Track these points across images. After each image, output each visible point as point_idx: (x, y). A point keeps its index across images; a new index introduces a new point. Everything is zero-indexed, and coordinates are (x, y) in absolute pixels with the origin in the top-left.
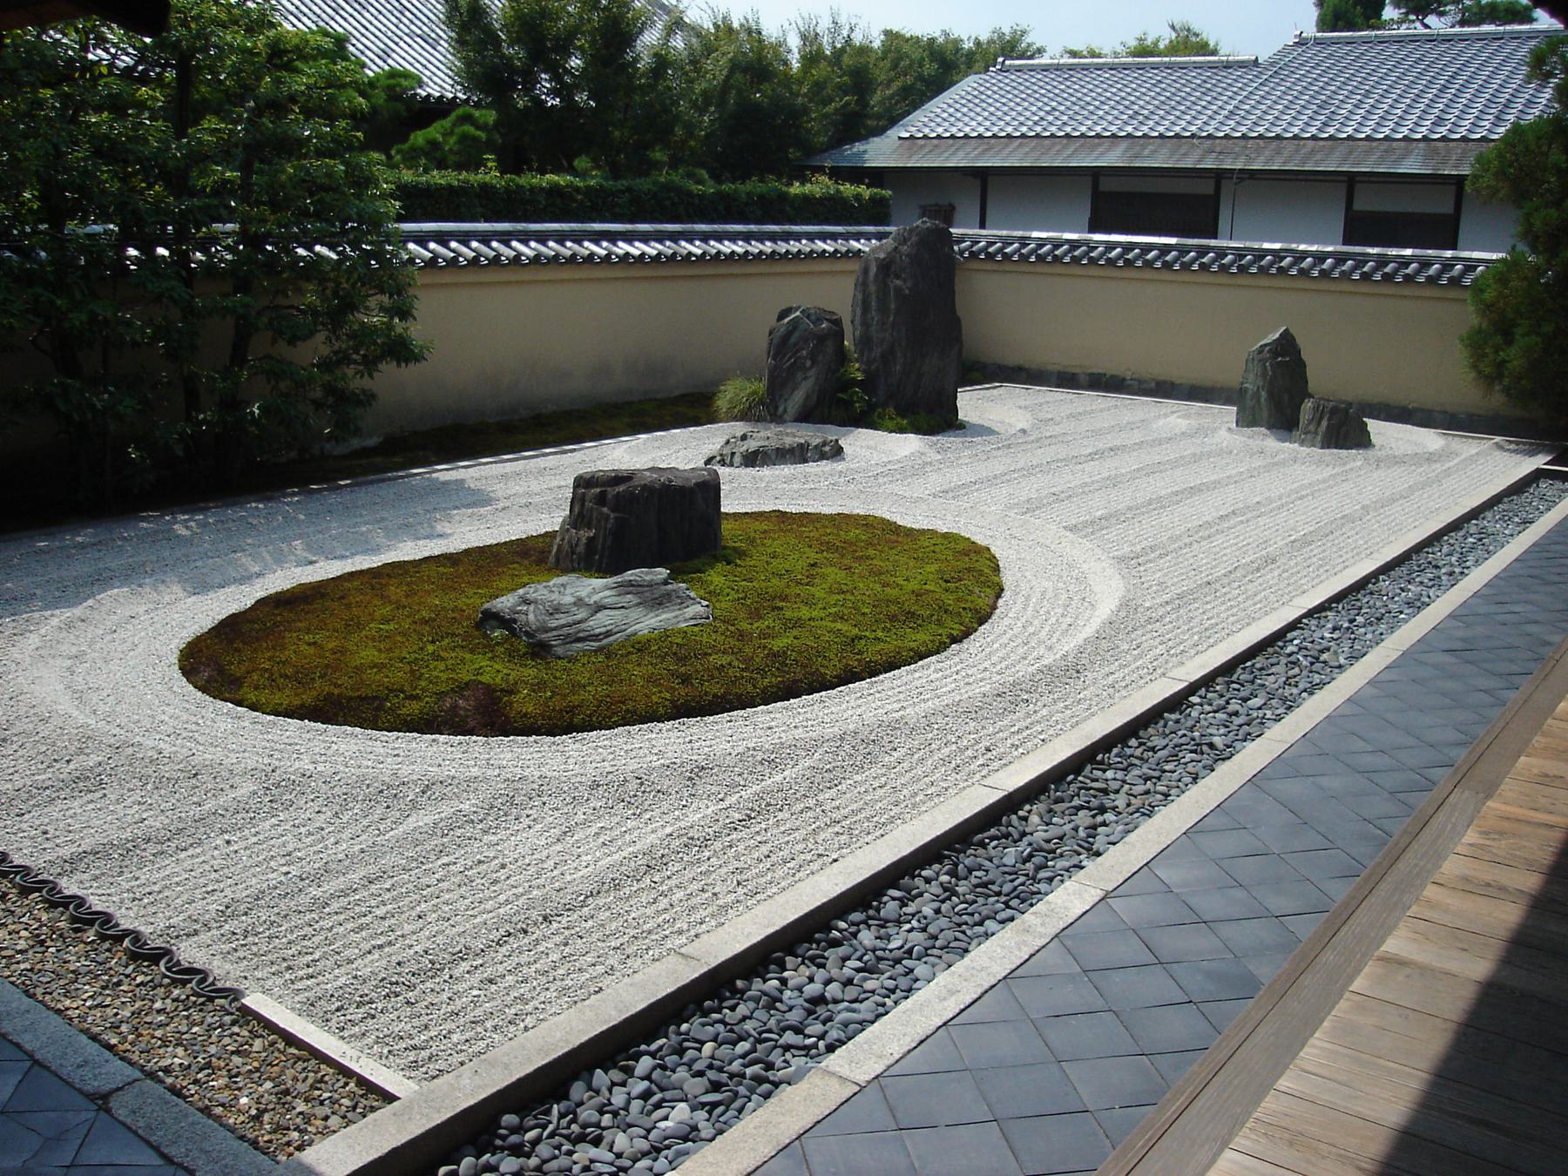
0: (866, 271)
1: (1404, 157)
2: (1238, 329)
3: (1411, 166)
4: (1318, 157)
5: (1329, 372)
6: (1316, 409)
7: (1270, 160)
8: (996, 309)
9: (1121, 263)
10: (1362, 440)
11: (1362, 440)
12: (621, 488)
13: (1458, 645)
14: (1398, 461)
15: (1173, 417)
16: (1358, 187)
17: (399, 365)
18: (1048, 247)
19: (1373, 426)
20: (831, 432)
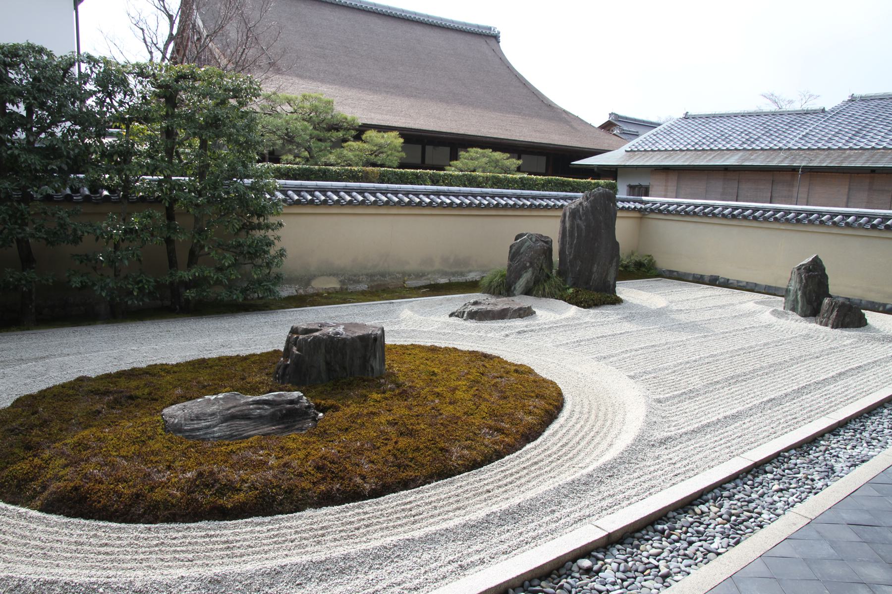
0: (565, 215)
2: (782, 255)
4: (852, 159)
5: (841, 285)
6: (830, 304)
10: (860, 323)
11: (860, 323)
13: (864, 518)
15: (748, 302)
16: (429, 149)
19: (869, 316)
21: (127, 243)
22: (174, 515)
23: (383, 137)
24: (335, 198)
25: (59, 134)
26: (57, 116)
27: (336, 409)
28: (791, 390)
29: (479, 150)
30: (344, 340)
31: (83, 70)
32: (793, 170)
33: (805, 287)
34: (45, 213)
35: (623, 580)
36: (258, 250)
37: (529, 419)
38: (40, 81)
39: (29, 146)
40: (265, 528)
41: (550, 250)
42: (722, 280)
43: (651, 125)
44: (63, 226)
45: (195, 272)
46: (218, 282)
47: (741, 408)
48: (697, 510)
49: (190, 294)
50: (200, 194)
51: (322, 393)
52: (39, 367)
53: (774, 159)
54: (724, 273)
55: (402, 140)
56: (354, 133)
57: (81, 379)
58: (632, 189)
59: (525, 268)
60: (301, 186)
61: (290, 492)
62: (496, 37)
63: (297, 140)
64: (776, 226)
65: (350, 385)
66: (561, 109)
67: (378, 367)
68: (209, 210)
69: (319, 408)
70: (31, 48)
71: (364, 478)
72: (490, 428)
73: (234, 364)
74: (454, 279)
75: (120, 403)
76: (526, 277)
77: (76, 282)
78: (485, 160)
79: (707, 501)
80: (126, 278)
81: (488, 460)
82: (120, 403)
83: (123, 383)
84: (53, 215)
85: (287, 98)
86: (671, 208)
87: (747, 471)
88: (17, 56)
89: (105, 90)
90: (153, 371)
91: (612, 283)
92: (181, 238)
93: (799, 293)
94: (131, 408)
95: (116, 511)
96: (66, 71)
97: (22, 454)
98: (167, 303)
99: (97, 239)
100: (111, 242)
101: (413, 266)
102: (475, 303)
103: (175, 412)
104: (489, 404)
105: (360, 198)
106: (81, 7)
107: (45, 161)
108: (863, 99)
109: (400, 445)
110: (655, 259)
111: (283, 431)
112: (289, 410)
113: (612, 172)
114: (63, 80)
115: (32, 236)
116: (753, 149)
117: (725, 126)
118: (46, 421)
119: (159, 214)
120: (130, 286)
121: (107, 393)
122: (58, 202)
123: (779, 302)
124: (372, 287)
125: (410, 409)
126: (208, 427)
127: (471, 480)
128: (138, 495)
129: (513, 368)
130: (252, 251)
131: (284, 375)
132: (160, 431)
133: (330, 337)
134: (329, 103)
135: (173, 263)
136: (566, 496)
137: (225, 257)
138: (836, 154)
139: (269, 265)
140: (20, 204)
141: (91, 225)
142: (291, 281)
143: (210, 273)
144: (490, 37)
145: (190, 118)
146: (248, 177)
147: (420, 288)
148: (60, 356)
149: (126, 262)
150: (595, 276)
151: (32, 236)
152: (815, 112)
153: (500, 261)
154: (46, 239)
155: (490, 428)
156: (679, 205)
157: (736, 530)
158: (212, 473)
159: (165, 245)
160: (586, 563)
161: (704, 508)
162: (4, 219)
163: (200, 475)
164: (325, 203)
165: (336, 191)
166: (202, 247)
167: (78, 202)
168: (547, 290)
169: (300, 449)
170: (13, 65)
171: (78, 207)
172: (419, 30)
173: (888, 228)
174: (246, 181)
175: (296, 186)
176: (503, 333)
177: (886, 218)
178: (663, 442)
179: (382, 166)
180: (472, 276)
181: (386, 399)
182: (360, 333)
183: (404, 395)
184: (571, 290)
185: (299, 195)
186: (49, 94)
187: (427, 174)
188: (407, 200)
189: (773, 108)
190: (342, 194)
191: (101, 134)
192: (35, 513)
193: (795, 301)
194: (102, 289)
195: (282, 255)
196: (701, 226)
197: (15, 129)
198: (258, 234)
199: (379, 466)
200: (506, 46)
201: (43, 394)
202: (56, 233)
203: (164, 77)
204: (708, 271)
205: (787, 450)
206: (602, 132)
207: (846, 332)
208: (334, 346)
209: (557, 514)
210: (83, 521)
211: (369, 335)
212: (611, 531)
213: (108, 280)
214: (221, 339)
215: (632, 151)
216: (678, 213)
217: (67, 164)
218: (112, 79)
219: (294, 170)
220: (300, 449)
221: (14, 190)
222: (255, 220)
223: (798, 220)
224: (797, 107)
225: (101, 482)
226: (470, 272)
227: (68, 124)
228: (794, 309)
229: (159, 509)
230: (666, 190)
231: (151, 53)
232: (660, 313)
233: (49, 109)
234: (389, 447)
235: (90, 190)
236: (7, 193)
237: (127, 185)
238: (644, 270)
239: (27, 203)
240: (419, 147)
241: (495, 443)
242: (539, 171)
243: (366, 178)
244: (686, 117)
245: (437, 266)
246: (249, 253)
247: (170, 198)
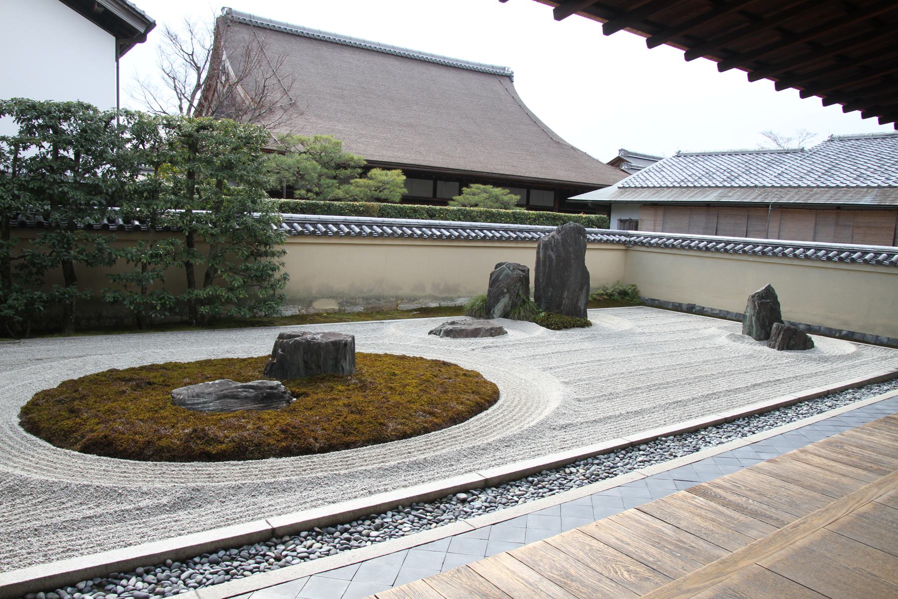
0: (539, 246)
1: (864, 196)
2: (740, 283)
3: (867, 201)
5: (791, 311)
6: (777, 328)
7: (765, 198)
9: (741, 252)
10: (807, 345)
11: (807, 345)
14: (826, 359)
16: (439, 183)
18: (770, 248)
19: (815, 338)
21: (152, 265)
22: (174, 456)
23: (387, 175)
24: (335, 229)
25: (100, 175)
26: (100, 158)
27: (306, 395)
28: (700, 394)
29: (482, 186)
30: (319, 344)
31: (121, 122)
32: (764, 206)
33: (759, 313)
34: (87, 239)
35: (486, 507)
36: (262, 276)
37: (460, 407)
38: (86, 132)
39: (77, 185)
40: (238, 468)
42: (698, 308)
43: (653, 160)
44: (101, 250)
45: (209, 291)
46: (229, 301)
47: (645, 407)
48: (567, 471)
49: (204, 310)
50: (215, 224)
51: (299, 384)
52: (79, 362)
53: (749, 196)
55: (404, 177)
56: (360, 171)
57: (112, 371)
58: (623, 223)
59: (502, 294)
60: (305, 219)
61: (258, 445)
62: (510, 77)
63: (307, 177)
64: (745, 258)
65: (322, 380)
67: (348, 367)
68: (222, 239)
69: (294, 395)
70: (81, 105)
71: (316, 439)
72: (424, 411)
73: (234, 364)
74: (444, 304)
75: (140, 387)
76: (504, 301)
77: (109, 297)
78: (485, 195)
79: (579, 466)
80: (151, 295)
81: (416, 433)
82: (140, 387)
83: (144, 374)
84: (93, 241)
85: (300, 140)
86: (653, 241)
87: (624, 448)
88: (70, 111)
89: (138, 137)
90: (167, 367)
91: (582, 308)
92: (197, 262)
93: (754, 318)
94: (149, 390)
95: (133, 452)
96: (107, 123)
97: (67, 415)
98: (186, 318)
99: (128, 261)
100: (140, 265)
101: (406, 291)
102: (453, 323)
103: (181, 392)
104: (429, 396)
105: (357, 230)
106: (121, 60)
107: (88, 197)
108: (841, 139)
109: (348, 419)
110: (639, 288)
111: (263, 408)
112: (268, 394)
113: (606, 207)
114: (105, 131)
115: (76, 258)
118: (84, 396)
119: (180, 242)
120: (154, 302)
121: (131, 380)
122: (97, 230)
123: (738, 327)
124: (368, 309)
125: (365, 397)
126: (205, 403)
127: (399, 446)
128: (149, 442)
129: (462, 372)
130: (258, 274)
131: (271, 370)
132: (169, 404)
133: (307, 341)
134: (338, 144)
135: (191, 284)
136: (465, 456)
137: (235, 279)
138: (804, 191)
139: (273, 286)
140: (66, 232)
141: (124, 251)
142: (294, 302)
143: (223, 293)
144: (506, 77)
145: (209, 162)
146: (256, 211)
147: (411, 311)
149: (152, 281)
150: (566, 301)
151: (76, 258)
152: (795, 152)
153: (482, 288)
154: (87, 261)
155: (424, 411)
156: (660, 238)
158: (203, 430)
159: (184, 268)
160: (462, 496)
161: (574, 470)
162: (54, 243)
163: (195, 431)
164: (325, 234)
165: (336, 224)
166: (216, 271)
167: (113, 231)
168: (522, 314)
169: (273, 419)
170: (67, 119)
171: (114, 235)
172: (435, 71)
173: (893, 264)
174: (255, 214)
175: (301, 219)
176: (470, 348)
177: (891, 254)
178: (564, 427)
179: (385, 201)
180: (460, 302)
181: (349, 390)
182: (333, 339)
183: (363, 387)
184: (543, 314)
185: (303, 227)
186: (94, 142)
187: (424, 209)
188: (400, 232)
189: (773, 146)
190: (342, 226)
191: (135, 172)
192: (76, 453)
193: (751, 325)
194: (131, 303)
195: (285, 279)
197: (66, 170)
198: (264, 260)
199: (329, 432)
200: (520, 86)
201: (82, 380)
202: (94, 256)
203: (188, 128)
205: (666, 435)
206: (610, 168)
207: (786, 353)
208: (311, 348)
209: (454, 467)
210: (109, 458)
211: (340, 341)
212: (488, 477)
213: (136, 296)
214: (227, 347)
215: (624, 187)
216: (658, 246)
217: (106, 199)
218: (144, 128)
219: (302, 204)
220: (273, 419)
221: (62, 220)
222: (262, 249)
223: (764, 254)
225: (123, 434)
226: (460, 297)
227: (108, 166)
228: (749, 334)
229: (164, 452)
230: (655, 225)
231: (180, 99)
232: (621, 335)
233: (93, 154)
234: (340, 420)
235: (124, 221)
236: (57, 223)
237: (154, 216)
238: (624, 297)
239: (72, 231)
240: (431, 182)
241: (426, 422)
242: (545, 204)
243: (366, 212)
245: (429, 291)
246: (256, 276)
247: (190, 228)
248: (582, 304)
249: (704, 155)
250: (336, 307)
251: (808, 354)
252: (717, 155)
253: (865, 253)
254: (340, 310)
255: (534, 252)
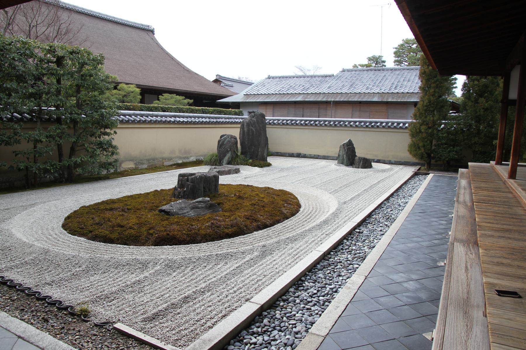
2: (334, 141)
3: (376, 99)
5: (360, 153)
7: (340, 98)
8: (277, 137)
10: (370, 166)
11: (370, 166)
12: (193, 177)
15: (323, 162)
17: (98, 61)
20: (237, 167)
32: (327, 103)
33: (347, 153)
41: (236, 143)
53: (318, 98)
54: (303, 151)
59: (228, 152)
62: (152, 31)
66: (194, 72)
74: (185, 161)
76: (228, 155)
93: (345, 156)
116: (308, 93)
117: (292, 82)
120: (48, 168)
135: (60, 155)
147: (171, 165)
148: (53, 200)
152: (330, 76)
156: (279, 120)
157: (391, 219)
168: (239, 162)
172: (110, 26)
189: (301, 74)
196: (290, 130)
200: (157, 36)
204: (296, 151)
206: (215, 84)
223: (336, 125)
224: (311, 73)
226: (191, 157)
228: (342, 163)
244: (269, 78)
245: (177, 154)
248: (265, 154)
249: (283, 77)
250: (134, 166)
251: (371, 169)
252: (290, 77)
253: (382, 123)
254: (136, 167)
255: (239, 130)
